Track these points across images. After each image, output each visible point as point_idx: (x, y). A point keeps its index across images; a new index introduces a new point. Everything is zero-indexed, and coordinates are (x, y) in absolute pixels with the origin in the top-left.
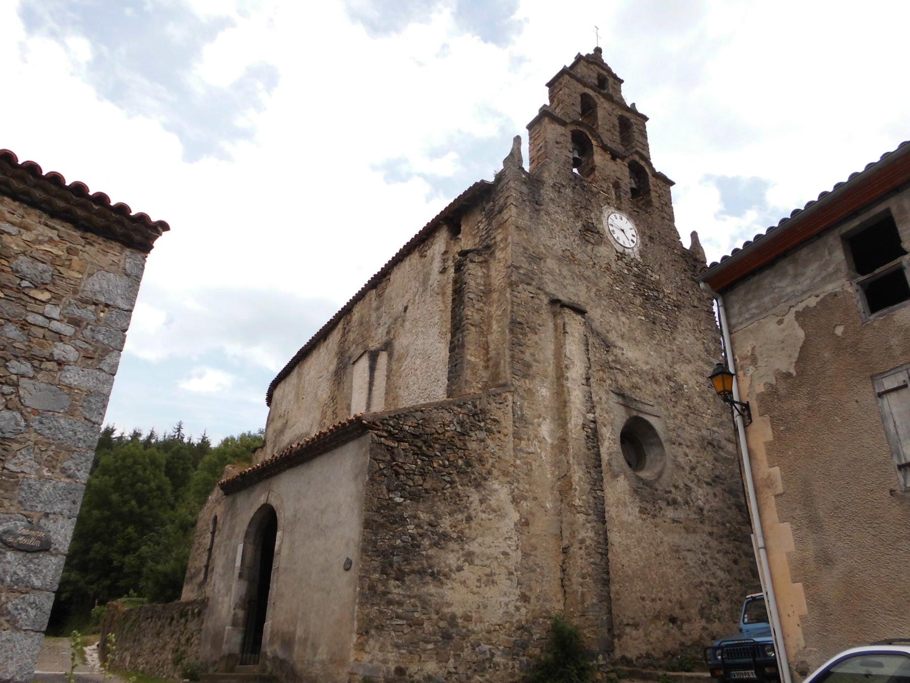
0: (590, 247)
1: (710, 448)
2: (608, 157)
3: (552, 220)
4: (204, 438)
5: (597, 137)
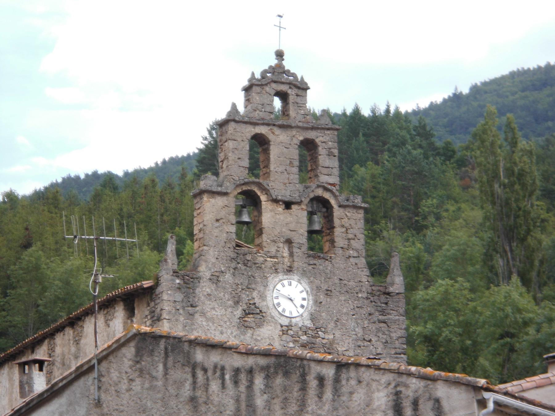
0: (250, 332)
1: (271, 408)
2: (280, 209)
3: (208, 320)
4: (344, 110)
5: (266, 191)
